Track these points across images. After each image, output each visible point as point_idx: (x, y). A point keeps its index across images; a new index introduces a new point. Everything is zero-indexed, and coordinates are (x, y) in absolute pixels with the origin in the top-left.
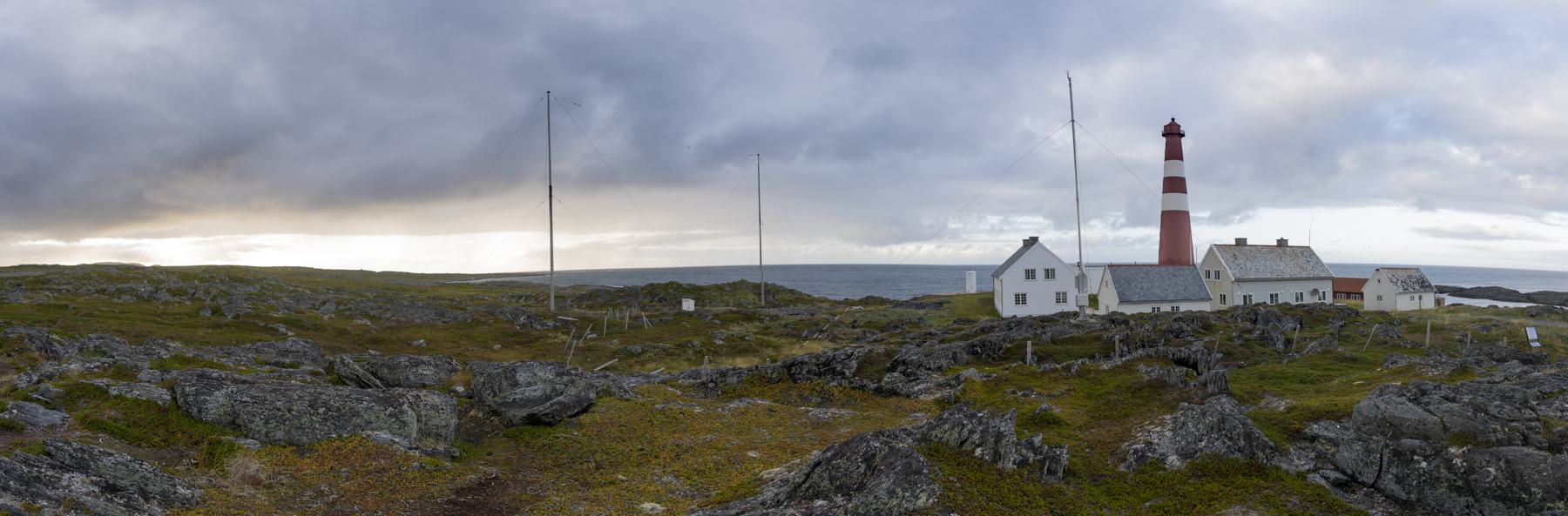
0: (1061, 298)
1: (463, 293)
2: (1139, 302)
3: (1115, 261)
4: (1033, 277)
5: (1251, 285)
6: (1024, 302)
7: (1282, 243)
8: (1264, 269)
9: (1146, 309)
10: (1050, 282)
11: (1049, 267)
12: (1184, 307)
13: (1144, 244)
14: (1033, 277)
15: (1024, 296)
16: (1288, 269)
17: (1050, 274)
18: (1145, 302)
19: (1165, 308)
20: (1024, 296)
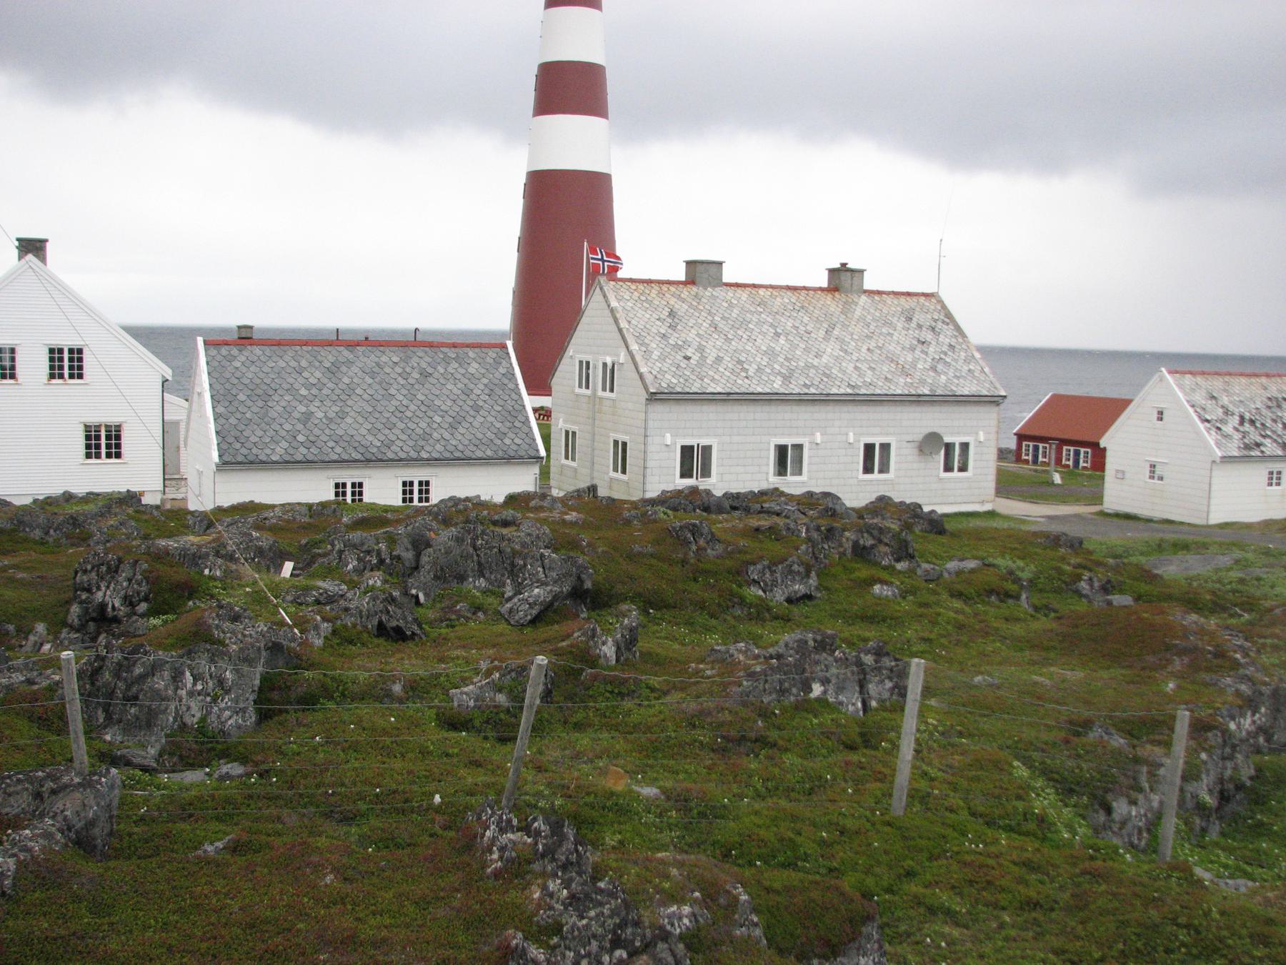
0: (103, 442)
1: (1132, 535)
2: (289, 464)
3: (265, 318)
4: (55, 354)
5: (804, 415)
6: (115, 451)
7: (843, 279)
8: (761, 358)
9: (313, 489)
10: (67, 389)
11: (66, 341)
12: (448, 485)
13: (427, 248)
14: (55, 354)
15: (77, 355)
16: (843, 359)
17: (66, 363)
18: (307, 464)
19: (383, 490)
20: (77, 355)
